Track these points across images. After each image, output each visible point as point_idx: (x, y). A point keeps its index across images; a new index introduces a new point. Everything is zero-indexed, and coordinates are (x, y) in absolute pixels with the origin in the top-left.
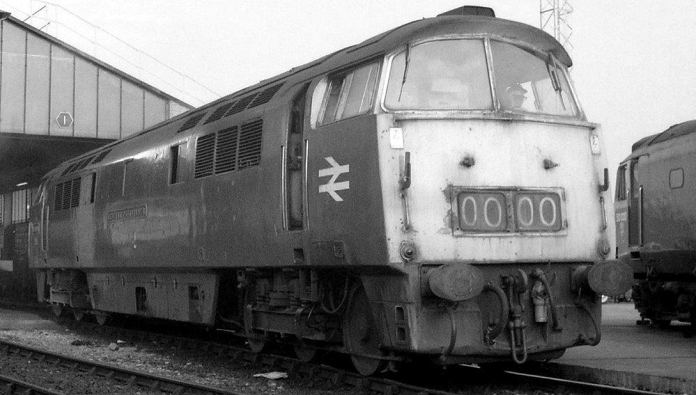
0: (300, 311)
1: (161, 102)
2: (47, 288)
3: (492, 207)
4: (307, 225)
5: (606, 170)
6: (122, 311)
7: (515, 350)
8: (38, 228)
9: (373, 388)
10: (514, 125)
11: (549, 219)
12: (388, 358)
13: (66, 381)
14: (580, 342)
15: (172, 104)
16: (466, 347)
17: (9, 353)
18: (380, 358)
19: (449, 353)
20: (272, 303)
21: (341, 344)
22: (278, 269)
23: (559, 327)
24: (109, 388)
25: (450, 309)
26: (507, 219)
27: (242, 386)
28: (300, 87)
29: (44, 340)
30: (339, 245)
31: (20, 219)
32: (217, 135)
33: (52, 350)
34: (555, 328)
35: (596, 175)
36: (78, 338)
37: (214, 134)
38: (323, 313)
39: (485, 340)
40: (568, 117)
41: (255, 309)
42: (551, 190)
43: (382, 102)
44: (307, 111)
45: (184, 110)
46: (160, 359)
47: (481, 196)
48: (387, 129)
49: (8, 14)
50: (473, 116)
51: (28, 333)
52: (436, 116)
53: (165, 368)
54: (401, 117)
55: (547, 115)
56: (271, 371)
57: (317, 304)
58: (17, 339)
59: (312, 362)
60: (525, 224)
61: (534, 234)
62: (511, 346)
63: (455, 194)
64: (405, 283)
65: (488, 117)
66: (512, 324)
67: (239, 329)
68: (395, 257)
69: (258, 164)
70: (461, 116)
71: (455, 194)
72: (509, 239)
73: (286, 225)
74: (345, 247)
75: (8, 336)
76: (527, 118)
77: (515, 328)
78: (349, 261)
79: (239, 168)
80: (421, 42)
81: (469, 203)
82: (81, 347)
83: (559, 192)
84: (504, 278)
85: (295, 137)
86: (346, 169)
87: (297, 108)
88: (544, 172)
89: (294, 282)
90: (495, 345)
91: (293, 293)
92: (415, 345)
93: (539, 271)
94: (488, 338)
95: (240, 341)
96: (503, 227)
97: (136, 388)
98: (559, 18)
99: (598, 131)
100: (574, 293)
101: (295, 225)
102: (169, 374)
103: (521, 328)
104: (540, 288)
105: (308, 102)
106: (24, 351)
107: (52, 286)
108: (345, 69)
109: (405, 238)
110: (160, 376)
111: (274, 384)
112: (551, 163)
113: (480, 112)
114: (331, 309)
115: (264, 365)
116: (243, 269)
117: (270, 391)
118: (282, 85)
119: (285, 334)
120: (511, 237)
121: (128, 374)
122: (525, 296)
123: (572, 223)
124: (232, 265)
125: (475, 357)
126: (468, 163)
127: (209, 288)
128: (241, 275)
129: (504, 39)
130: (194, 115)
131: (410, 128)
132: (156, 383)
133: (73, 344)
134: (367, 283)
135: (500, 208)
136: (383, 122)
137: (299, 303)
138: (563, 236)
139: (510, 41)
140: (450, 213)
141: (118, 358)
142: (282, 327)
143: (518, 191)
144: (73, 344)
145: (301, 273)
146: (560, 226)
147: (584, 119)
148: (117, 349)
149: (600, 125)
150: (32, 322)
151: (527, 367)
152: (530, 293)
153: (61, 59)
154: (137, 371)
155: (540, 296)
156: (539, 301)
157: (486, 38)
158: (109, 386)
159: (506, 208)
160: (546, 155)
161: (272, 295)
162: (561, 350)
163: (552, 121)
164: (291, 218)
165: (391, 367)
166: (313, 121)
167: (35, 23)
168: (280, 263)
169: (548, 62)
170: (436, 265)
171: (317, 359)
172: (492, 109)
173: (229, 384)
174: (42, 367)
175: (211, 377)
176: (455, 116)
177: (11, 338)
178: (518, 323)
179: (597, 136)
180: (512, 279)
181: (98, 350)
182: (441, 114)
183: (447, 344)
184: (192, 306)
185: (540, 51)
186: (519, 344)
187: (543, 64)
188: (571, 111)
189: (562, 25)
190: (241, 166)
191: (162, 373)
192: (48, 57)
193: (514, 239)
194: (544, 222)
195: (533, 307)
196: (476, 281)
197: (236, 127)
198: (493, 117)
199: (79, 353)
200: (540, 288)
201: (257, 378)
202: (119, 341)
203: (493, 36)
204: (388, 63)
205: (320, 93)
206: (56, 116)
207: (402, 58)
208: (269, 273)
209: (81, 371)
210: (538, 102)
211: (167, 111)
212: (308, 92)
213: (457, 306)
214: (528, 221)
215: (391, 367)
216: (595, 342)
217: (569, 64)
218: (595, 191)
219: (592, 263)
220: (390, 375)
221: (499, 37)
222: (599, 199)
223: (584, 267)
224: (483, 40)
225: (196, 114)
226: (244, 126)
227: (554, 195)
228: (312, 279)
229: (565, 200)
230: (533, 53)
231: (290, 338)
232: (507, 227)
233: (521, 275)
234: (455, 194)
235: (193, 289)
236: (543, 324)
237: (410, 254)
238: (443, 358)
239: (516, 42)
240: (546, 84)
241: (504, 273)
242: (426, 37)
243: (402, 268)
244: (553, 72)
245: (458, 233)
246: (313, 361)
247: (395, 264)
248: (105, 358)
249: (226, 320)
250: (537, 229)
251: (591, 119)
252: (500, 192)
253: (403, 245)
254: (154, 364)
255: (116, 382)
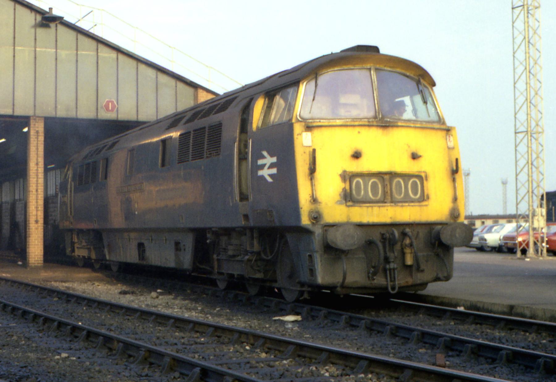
0: (247, 257)
1: (190, 90)
2: (73, 243)
3: (374, 185)
4: (251, 198)
5: (457, 160)
6: (129, 260)
7: (390, 284)
8: (65, 199)
9: (374, 328)
10: (390, 129)
11: (415, 193)
12: (304, 289)
13: (115, 324)
14: (437, 279)
15: (200, 92)
16: (356, 282)
17: (68, 301)
18: (299, 289)
19: (343, 286)
20: (230, 253)
21: (276, 281)
22: (233, 229)
23: (421, 269)
24: (152, 329)
25: (343, 256)
26: (385, 193)
27: (263, 328)
28: (248, 99)
29: (96, 290)
30: (271, 211)
31: (51, 193)
32: (192, 132)
33: (104, 298)
34: (419, 269)
35: (450, 162)
36: (124, 288)
37: (190, 132)
38: (264, 260)
39: (369, 277)
40: (433, 122)
41: (219, 258)
42: (417, 174)
43: (298, 114)
44: (250, 118)
45: (210, 97)
46: (193, 305)
47: (367, 178)
48: (301, 132)
49: (61, 18)
50: (361, 123)
51: (82, 284)
52: (334, 124)
53: (198, 313)
54: (310, 125)
55: (421, 122)
56: (288, 314)
57: (258, 253)
58: (74, 289)
59: (257, 295)
60: (397, 197)
61: (404, 204)
62: (387, 281)
63: (347, 177)
64: (313, 238)
65: (371, 124)
66: (388, 267)
67: (211, 273)
68: (305, 221)
69: (219, 154)
70: (353, 123)
71: (347, 177)
72: (386, 208)
73: (237, 198)
74: (274, 213)
75: (66, 287)
76: (400, 124)
77: (390, 270)
78: (278, 224)
79: (207, 157)
80: (326, 71)
81: (358, 183)
82: (128, 296)
83: (423, 175)
84: (383, 235)
85: (243, 136)
86: (274, 160)
87: (245, 116)
88: (412, 161)
89: (244, 238)
90: (375, 281)
91: (243, 245)
92: (320, 280)
93: (408, 230)
94: (371, 276)
95: (213, 283)
96: (382, 200)
97: (174, 329)
98: (528, 13)
99: (453, 132)
100: (433, 245)
101: (244, 197)
102: (201, 317)
103: (394, 269)
104: (407, 241)
105: (251, 112)
106: (80, 300)
107: (393, 262)
108: (277, 89)
109: (313, 207)
110: (194, 319)
111: (290, 326)
112: (417, 154)
113: (366, 120)
114: (268, 257)
115: (282, 310)
116: (210, 228)
117: (287, 332)
118: (236, 98)
119: (238, 275)
120: (388, 206)
121: (167, 318)
122: (398, 247)
123: (432, 196)
124: (202, 226)
125: (363, 289)
126: (357, 155)
127: (188, 242)
128: (209, 234)
129: (386, 68)
130: (177, 117)
131: (316, 132)
132: (191, 325)
133: (120, 293)
134: (289, 237)
135: (380, 186)
136: (298, 128)
137: (246, 252)
138: (426, 205)
139: (389, 69)
140: (344, 190)
141: (158, 305)
142: (236, 270)
143: (392, 175)
144: (120, 293)
145: (248, 232)
146: (424, 198)
147: (444, 123)
148: (157, 297)
149: (454, 128)
150: (86, 275)
151: (397, 296)
152: (402, 245)
153: (106, 55)
154: (175, 314)
155: (408, 247)
156: (408, 251)
157: (372, 68)
158: (152, 328)
159: (384, 187)
160: (414, 149)
161: (230, 247)
162: (424, 285)
163: (418, 125)
164: (241, 193)
165: (306, 296)
166: (254, 126)
167: (84, 25)
168: (234, 225)
169: (418, 83)
170: (333, 226)
171: (261, 293)
172: (375, 117)
173: (253, 325)
174: (96, 313)
175: (237, 319)
176: (348, 124)
177: (68, 288)
178: (392, 266)
179: (452, 135)
180: (388, 235)
181: (142, 298)
182: (339, 122)
183: (341, 280)
184: (177, 256)
185: (412, 75)
186: (393, 280)
187: (414, 84)
188: (434, 117)
189: (531, 20)
190: (208, 155)
191: (196, 317)
192: (95, 53)
193: (389, 208)
194: (411, 195)
195: (403, 254)
196: (358, 238)
197: (204, 128)
198: (375, 124)
199: (126, 300)
200: (407, 241)
201: (275, 320)
202: (159, 291)
203: (378, 66)
204: (302, 87)
205: (259, 106)
206: (103, 101)
207: (313, 83)
208: (228, 232)
209: (127, 315)
210: (415, 111)
211: (196, 97)
212: (252, 103)
213: (348, 253)
214: (401, 194)
215: (306, 296)
216: (447, 278)
217: (433, 84)
218: (449, 173)
219: (447, 224)
220: (305, 302)
221: (382, 67)
222: (452, 179)
223: (439, 227)
224: (370, 69)
225: (179, 116)
226: (211, 127)
227: (419, 177)
228: (255, 235)
229: (427, 180)
230: (407, 76)
231: (241, 277)
232: (384, 199)
233: (393, 231)
234: (347, 177)
235: (177, 244)
236: (410, 267)
237: (316, 217)
238: (339, 289)
239: (394, 70)
240: (418, 99)
241: (383, 231)
242: (330, 68)
243: (311, 228)
244: (421, 91)
245: (349, 203)
246: (258, 295)
247: (306, 225)
248: (147, 305)
249: (202, 267)
250: (407, 200)
251: (449, 123)
252: (379, 175)
253: (311, 212)
254: (189, 309)
255: (157, 324)
